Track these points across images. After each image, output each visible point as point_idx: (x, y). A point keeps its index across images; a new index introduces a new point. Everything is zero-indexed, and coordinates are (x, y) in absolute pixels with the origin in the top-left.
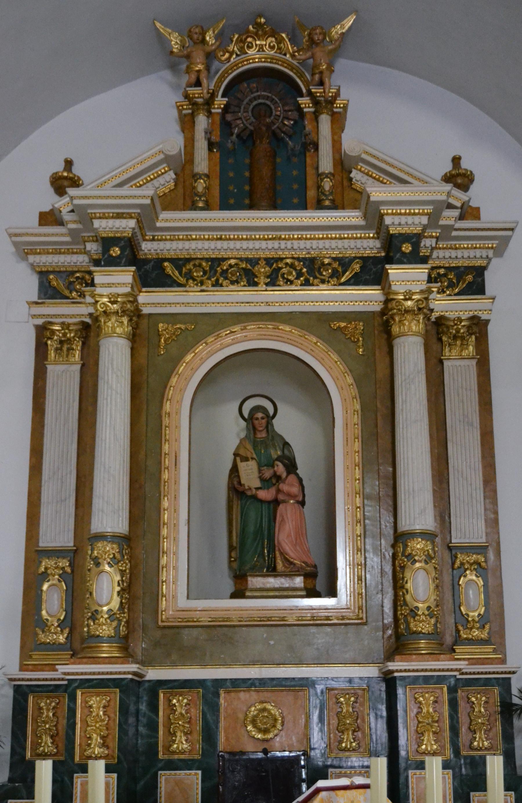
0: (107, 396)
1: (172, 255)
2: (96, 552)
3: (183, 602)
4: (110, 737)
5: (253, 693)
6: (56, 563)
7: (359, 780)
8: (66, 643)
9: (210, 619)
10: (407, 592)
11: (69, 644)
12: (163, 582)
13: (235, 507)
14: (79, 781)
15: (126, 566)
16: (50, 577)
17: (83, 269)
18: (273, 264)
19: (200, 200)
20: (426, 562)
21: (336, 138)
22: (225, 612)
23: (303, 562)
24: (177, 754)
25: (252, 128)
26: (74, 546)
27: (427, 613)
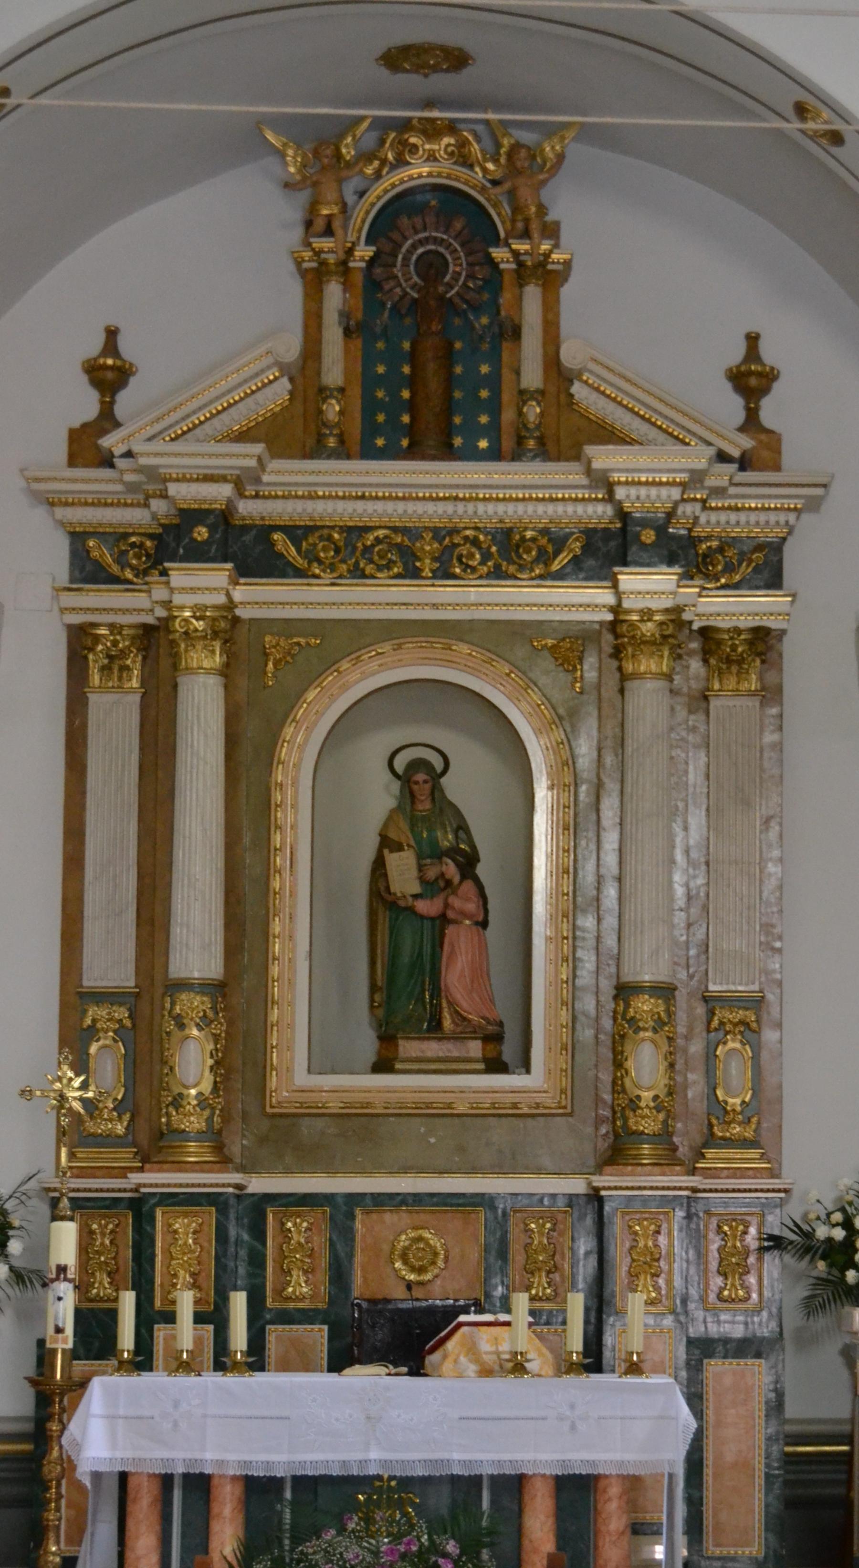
0: (192, 768)
1: (285, 521)
2: (178, 1007)
3: (302, 1078)
4: (203, 1274)
5: (404, 1215)
6: (109, 1014)
7: (503, 1317)
8: (126, 1135)
9: (342, 1105)
10: (627, 1073)
11: (130, 1137)
12: (272, 1047)
13: (380, 921)
14: (162, 1334)
15: (219, 1028)
16: (101, 1034)
17: (142, 531)
18: (444, 538)
19: (331, 434)
20: (655, 1031)
21: (550, 316)
22: (363, 1095)
23: (482, 1018)
24: (294, 1301)
25: (416, 295)
26: (136, 987)
27: (652, 1104)
